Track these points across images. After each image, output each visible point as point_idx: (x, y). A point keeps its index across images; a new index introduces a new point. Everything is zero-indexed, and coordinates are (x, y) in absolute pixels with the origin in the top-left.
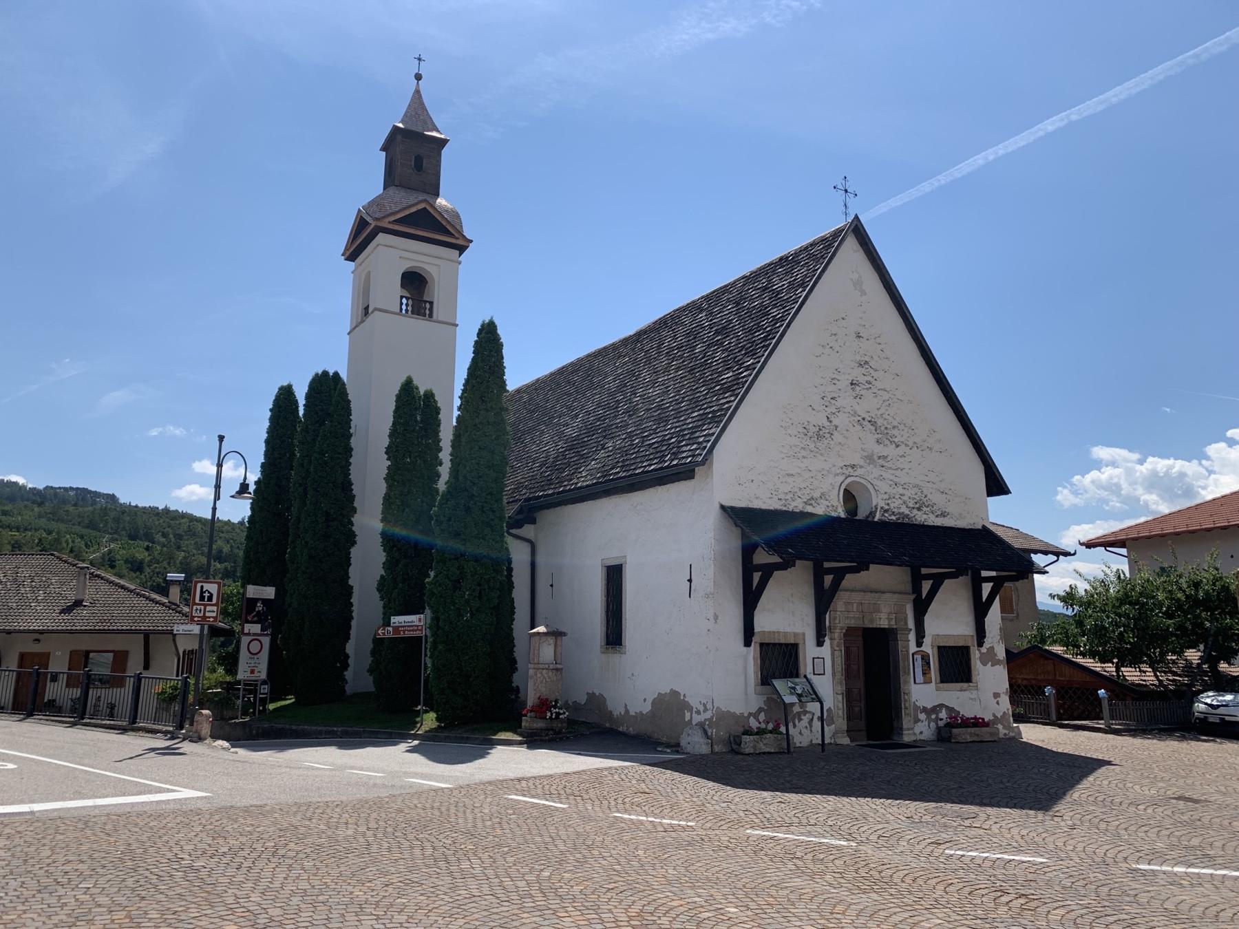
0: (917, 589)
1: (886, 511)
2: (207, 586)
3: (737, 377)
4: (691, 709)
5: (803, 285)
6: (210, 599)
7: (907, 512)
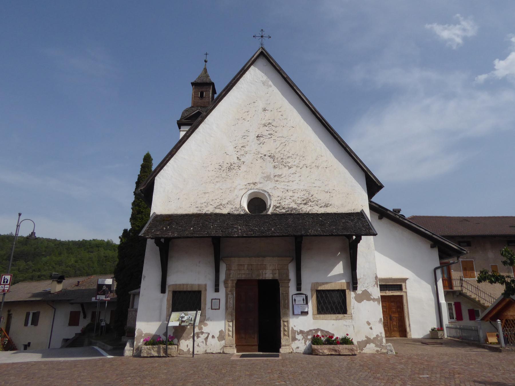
6: (7, 282)
7: (295, 206)
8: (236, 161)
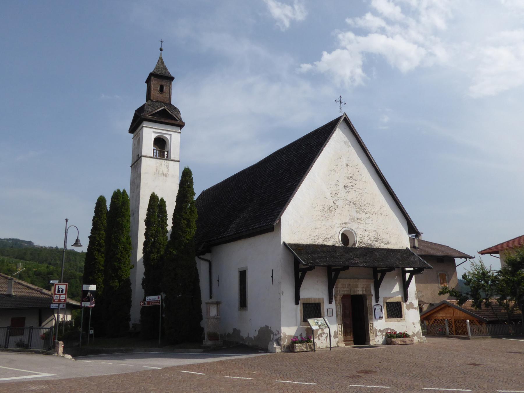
0: (375, 277)
1: (361, 243)
2: (61, 286)
4: (273, 333)
6: (62, 291)
7: (371, 243)
8: (333, 205)
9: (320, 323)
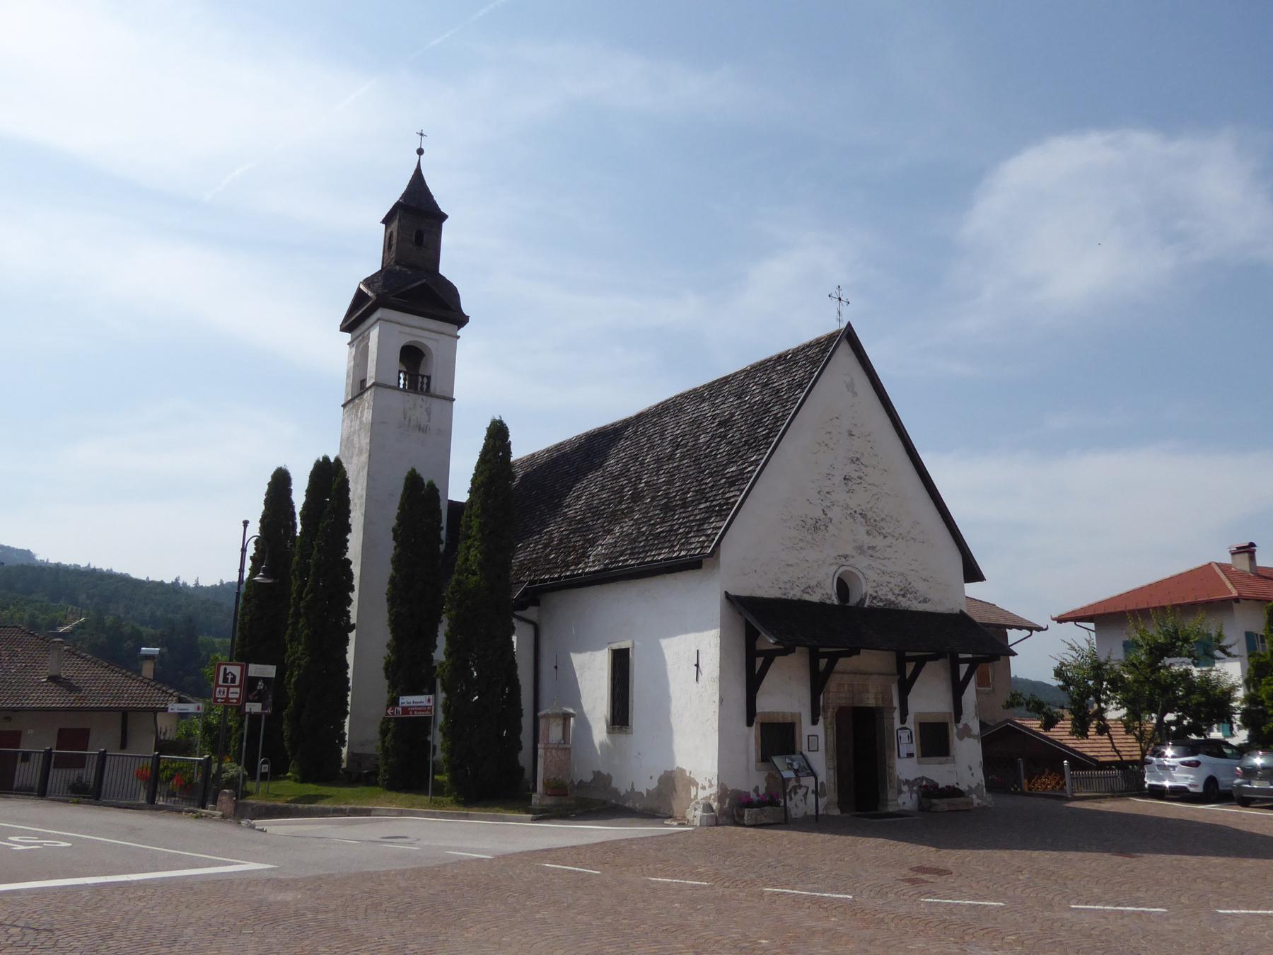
0: (901, 669)
1: (875, 598)
2: (230, 669)
3: (741, 472)
4: (696, 784)
5: (800, 386)
6: (233, 680)
7: (893, 598)
9: (796, 767)
